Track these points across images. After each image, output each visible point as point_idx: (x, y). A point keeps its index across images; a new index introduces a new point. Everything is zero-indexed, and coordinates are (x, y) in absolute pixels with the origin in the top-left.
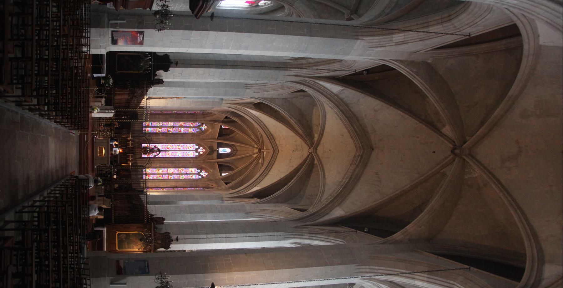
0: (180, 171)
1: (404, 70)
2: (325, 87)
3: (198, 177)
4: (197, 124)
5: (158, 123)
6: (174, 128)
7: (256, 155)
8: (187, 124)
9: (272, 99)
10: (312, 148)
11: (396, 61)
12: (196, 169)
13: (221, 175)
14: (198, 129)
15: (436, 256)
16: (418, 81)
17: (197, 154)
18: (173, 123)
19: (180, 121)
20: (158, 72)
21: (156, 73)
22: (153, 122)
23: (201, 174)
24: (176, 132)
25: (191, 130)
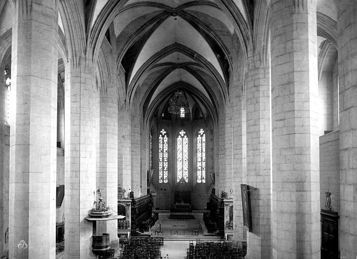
4: (161, 137)
17: (185, 136)
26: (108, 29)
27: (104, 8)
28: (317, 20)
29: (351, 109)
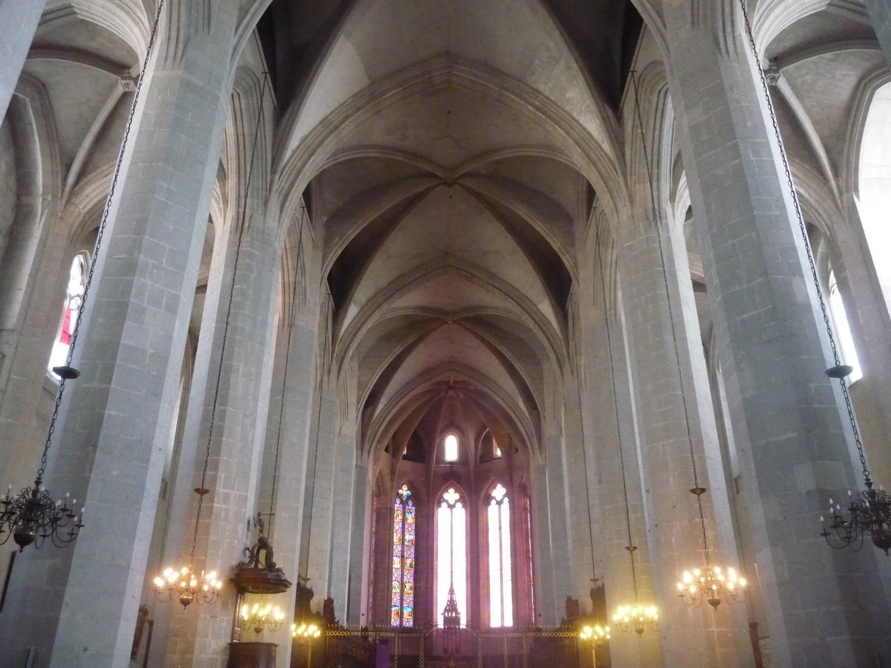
4: (397, 506)
5: (394, 591)
6: (404, 556)
7: (460, 393)
8: (397, 526)
9: (361, 386)
11: (323, 263)
14: (407, 504)
15: (592, 210)
16: (352, 233)
18: (394, 558)
19: (390, 544)
22: (391, 601)
25: (410, 518)
27: (314, 129)
28: (690, 268)
29: (764, 652)
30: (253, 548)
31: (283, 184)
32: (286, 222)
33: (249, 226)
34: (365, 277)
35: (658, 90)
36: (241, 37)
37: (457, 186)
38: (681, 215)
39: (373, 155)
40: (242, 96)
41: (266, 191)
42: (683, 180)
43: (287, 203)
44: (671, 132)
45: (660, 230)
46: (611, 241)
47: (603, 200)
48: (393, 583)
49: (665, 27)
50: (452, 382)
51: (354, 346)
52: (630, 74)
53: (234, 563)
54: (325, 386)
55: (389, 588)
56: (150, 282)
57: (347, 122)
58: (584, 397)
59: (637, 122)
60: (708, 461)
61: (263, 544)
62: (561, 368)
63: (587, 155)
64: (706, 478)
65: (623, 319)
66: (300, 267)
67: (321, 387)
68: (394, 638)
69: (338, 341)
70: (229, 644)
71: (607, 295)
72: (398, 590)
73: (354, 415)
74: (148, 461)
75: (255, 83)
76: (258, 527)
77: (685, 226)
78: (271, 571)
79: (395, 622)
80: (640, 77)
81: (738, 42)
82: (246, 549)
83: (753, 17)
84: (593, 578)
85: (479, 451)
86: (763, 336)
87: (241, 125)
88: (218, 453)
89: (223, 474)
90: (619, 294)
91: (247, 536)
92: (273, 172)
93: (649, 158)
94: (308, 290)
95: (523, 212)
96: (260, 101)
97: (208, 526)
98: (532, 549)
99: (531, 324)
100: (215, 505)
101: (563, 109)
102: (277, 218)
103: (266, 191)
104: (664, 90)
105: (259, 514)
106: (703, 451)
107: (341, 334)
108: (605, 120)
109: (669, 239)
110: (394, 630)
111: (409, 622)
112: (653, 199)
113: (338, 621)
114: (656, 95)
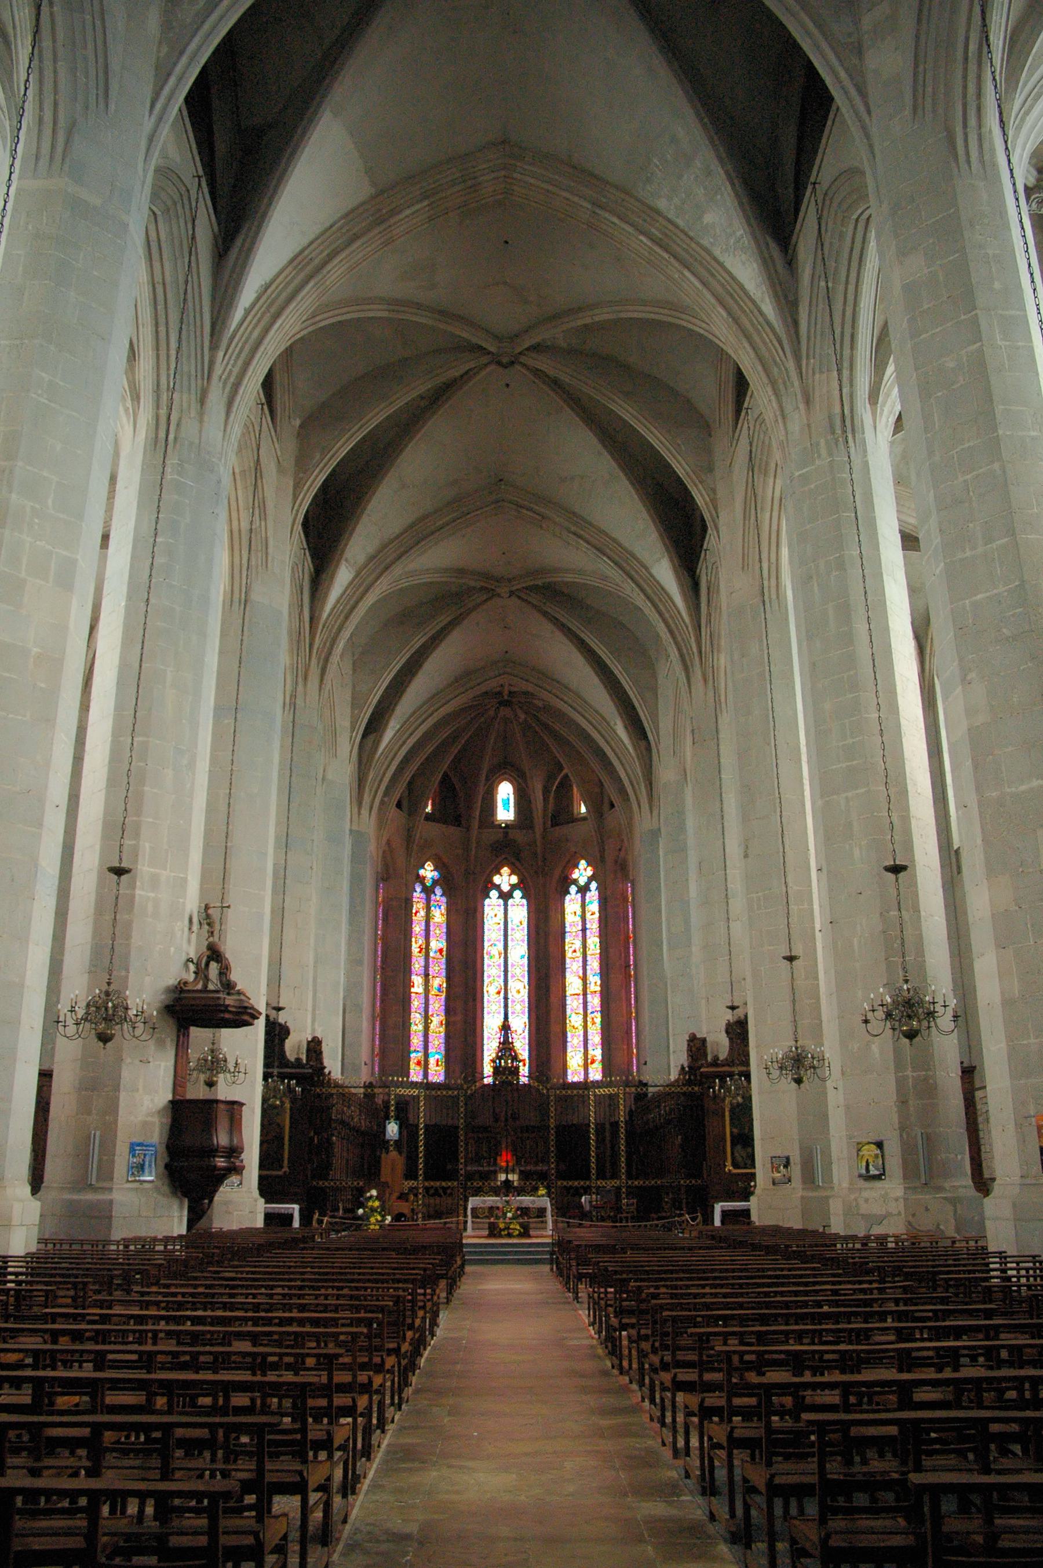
0: (575, 951)
1: (318, 479)
2: (338, 601)
3: (593, 894)
4: (418, 894)
5: (413, 1028)
8: (418, 928)
9: (356, 703)
10: (498, 590)
11: (295, 498)
12: (568, 898)
13: (584, 819)
14: (434, 892)
16: (342, 448)
17: (518, 894)
20: (288, 1054)
21: (293, 1060)
23: (582, 881)
24: (444, 967)
25: (439, 916)
26: (270, 371)
30: (199, 959)
31: (230, 367)
32: (236, 430)
33: (176, 438)
34: (365, 519)
35: (855, 217)
36: (160, 119)
37: (518, 367)
38: (887, 426)
39: (379, 314)
40: (160, 219)
41: (203, 379)
42: (890, 369)
43: (238, 398)
44: (874, 287)
45: (852, 450)
46: (773, 465)
47: (760, 395)
48: (412, 1016)
49: (869, 112)
50: (506, 693)
51: (346, 634)
52: (810, 188)
53: (172, 981)
54: (299, 702)
55: (406, 1024)
56: (29, 539)
57: (335, 261)
58: (725, 720)
59: (820, 268)
60: (913, 822)
61: (215, 954)
62: (686, 669)
63: (736, 321)
64: (908, 845)
65: (790, 594)
66: (258, 506)
67: (293, 705)
68: (418, 1097)
69: (320, 627)
70: (171, 1102)
71: (764, 556)
72: (421, 1027)
73: (346, 747)
74: (40, 825)
75: (181, 195)
76: (206, 927)
77: (892, 443)
78: (229, 994)
79: (416, 1075)
80: (826, 194)
81: (986, 146)
82: (188, 960)
83: (1013, 100)
84: (730, 1004)
85: (551, 806)
86: (1004, 630)
87: (159, 267)
88: (139, 813)
89: (147, 845)
90: (785, 552)
91: (189, 941)
92: (214, 347)
93: (838, 331)
94: (271, 543)
95: (626, 411)
96: (190, 226)
97: (129, 925)
98: (635, 961)
99: (640, 600)
100: (138, 892)
101: (698, 244)
102: (222, 428)
103: (203, 379)
104: (865, 216)
105: (207, 907)
106: (906, 808)
107: (325, 615)
108: (766, 263)
109: (866, 465)
110: (415, 1085)
111: (437, 1074)
112: (842, 400)
113: (330, 1073)
114: (851, 226)
